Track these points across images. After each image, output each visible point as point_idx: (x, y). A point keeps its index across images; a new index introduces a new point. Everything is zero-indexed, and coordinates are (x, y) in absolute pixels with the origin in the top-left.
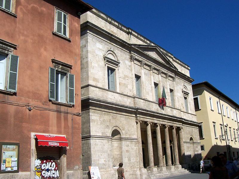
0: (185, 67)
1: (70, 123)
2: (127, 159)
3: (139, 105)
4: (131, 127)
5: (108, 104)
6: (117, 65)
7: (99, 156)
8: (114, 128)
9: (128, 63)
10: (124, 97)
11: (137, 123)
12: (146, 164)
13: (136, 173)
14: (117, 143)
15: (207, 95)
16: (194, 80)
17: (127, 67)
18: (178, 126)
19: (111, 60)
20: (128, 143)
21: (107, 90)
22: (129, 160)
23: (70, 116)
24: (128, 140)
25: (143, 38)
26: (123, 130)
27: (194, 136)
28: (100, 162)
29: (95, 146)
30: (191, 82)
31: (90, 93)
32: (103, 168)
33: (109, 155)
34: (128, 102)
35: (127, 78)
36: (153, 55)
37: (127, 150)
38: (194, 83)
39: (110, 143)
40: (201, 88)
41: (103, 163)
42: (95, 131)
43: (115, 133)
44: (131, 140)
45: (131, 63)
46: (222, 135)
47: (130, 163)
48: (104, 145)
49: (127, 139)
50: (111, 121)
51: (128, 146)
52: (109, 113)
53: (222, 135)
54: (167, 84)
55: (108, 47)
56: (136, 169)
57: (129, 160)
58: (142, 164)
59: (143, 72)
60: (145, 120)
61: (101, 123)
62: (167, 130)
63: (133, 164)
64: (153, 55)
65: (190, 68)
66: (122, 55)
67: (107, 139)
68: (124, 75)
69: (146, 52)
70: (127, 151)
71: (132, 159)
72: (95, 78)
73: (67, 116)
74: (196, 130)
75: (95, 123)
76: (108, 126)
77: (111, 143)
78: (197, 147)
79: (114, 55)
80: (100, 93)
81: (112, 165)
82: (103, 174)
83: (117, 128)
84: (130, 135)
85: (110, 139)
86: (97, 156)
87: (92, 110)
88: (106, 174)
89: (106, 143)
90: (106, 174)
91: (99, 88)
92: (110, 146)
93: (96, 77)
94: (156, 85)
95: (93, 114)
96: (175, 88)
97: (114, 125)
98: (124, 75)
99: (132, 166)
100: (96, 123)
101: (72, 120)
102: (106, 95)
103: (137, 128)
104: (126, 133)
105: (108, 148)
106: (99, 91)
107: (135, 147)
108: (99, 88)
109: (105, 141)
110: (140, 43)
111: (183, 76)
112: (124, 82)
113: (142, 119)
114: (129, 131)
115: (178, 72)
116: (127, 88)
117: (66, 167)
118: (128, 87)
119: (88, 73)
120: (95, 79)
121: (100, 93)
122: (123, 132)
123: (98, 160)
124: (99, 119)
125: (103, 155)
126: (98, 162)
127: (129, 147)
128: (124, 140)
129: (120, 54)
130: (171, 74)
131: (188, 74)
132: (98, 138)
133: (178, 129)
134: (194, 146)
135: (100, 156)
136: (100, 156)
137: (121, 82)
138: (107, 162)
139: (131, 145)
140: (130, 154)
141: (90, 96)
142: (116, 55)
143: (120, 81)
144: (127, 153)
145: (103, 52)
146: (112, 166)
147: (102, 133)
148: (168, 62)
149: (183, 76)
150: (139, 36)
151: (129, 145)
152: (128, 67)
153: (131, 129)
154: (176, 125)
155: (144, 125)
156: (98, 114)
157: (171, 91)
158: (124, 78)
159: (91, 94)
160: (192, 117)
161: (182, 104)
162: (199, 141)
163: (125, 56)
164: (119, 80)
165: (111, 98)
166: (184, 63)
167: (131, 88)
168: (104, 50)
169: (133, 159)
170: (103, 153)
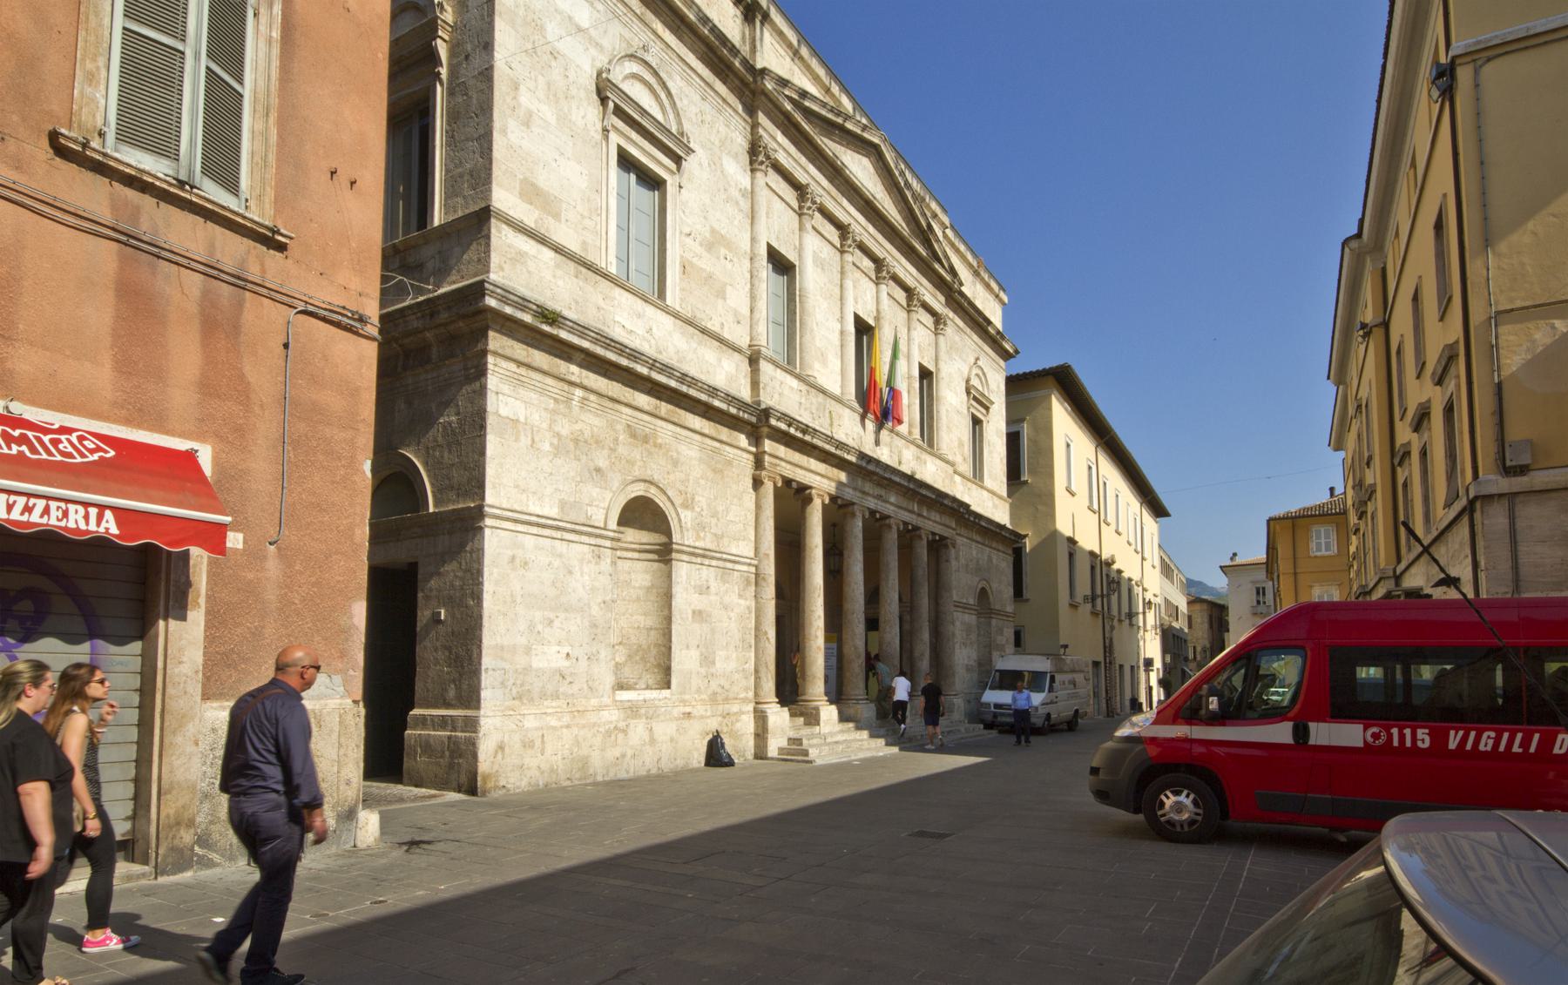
0: (988, 286)
1: (261, 374)
2: (694, 654)
3: (776, 396)
4: (724, 509)
5: (607, 347)
6: (678, 160)
7: (531, 627)
8: (638, 490)
9: (736, 170)
10: (700, 343)
11: (757, 483)
12: (789, 689)
13: (738, 725)
14: (646, 572)
15: (1062, 421)
16: (1017, 352)
17: (723, 192)
18: (938, 529)
19: (644, 112)
20: (707, 574)
21: (606, 276)
22: (707, 660)
23: (263, 318)
24: (707, 562)
25: (821, 72)
26: (686, 506)
27: (994, 586)
28: (538, 663)
29: (514, 569)
30: (1006, 355)
31: (495, 259)
32: (556, 696)
33: (595, 626)
34: (724, 374)
35: (723, 251)
36: (860, 168)
37: (700, 612)
38: (1022, 366)
39: (606, 564)
40: (1033, 394)
41: (554, 665)
42: (517, 486)
43: (643, 514)
44: (721, 564)
45: (753, 178)
46: (1094, 598)
47: (709, 677)
48: (570, 572)
49: (704, 555)
50: (621, 449)
51: (704, 590)
52: (610, 404)
53: (1094, 598)
54: (910, 342)
55: (628, 35)
56: (735, 708)
57: (707, 660)
58: (769, 685)
59: (814, 253)
60: (802, 477)
61: (558, 451)
62: (891, 540)
63: (722, 682)
64: (860, 168)
65: (1006, 299)
66: (708, 118)
67: (593, 541)
68: (713, 231)
69: (831, 146)
70: (699, 615)
71: (721, 654)
72: (533, 185)
73: (240, 305)
74: (1004, 564)
75: (517, 440)
76: (598, 470)
77: (614, 563)
78: (1000, 632)
79: (663, 96)
80: (560, 283)
81: (609, 680)
82: (554, 728)
83: (653, 493)
84: (718, 537)
85: (608, 543)
86: (522, 626)
87: (504, 364)
88: (568, 727)
89: (581, 561)
90: (568, 727)
91: (558, 250)
92: (604, 580)
93: (543, 180)
94: (864, 330)
95: (505, 388)
96: (942, 365)
97: (637, 473)
98: (713, 231)
99: (719, 690)
100: (525, 441)
101: (286, 346)
102: (601, 303)
103: (758, 507)
104: (701, 527)
105: (593, 589)
106: (557, 266)
107: (742, 602)
108: (558, 250)
109: (577, 551)
110: (803, 81)
111: (977, 321)
112: (706, 263)
113: (790, 472)
114: (714, 515)
115: (962, 294)
116: (720, 302)
117: (196, 689)
118: (724, 299)
119: (490, 143)
120: (531, 192)
121: (560, 283)
122: (687, 516)
123: (528, 650)
124: (545, 425)
125: (557, 623)
126: (521, 661)
127: (713, 598)
128: (685, 557)
129: (694, 110)
130: (928, 299)
131: (994, 313)
132: (535, 530)
133: (938, 546)
134: (989, 624)
135: (540, 627)
136: (540, 627)
137: (691, 263)
138: (583, 663)
139: (723, 589)
140: (713, 631)
141: (493, 277)
142: (673, 104)
143: (688, 255)
144: (696, 626)
145: (593, 51)
146: (608, 687)
147: (563, 505)
148: (926, 235)
149: (977, 321)
150: (804, 51)
151: (713, 585)
152: (736, 194)
153: (727, 510)
154: (932, 523)
155: (793, 497)
156: (543, 392)
157: (925, 375)
158: (710, 247)
159: (502, 269)
160: (995, 506)
161: (961, 444)
162: (1010, 609)
163: (722, 129)
164: (683, 245)
165: (632, 323)
166: (990, 269)
167: (739, 302)
168: (605, 43)
169: (727, 658)
170: (562, 615)
